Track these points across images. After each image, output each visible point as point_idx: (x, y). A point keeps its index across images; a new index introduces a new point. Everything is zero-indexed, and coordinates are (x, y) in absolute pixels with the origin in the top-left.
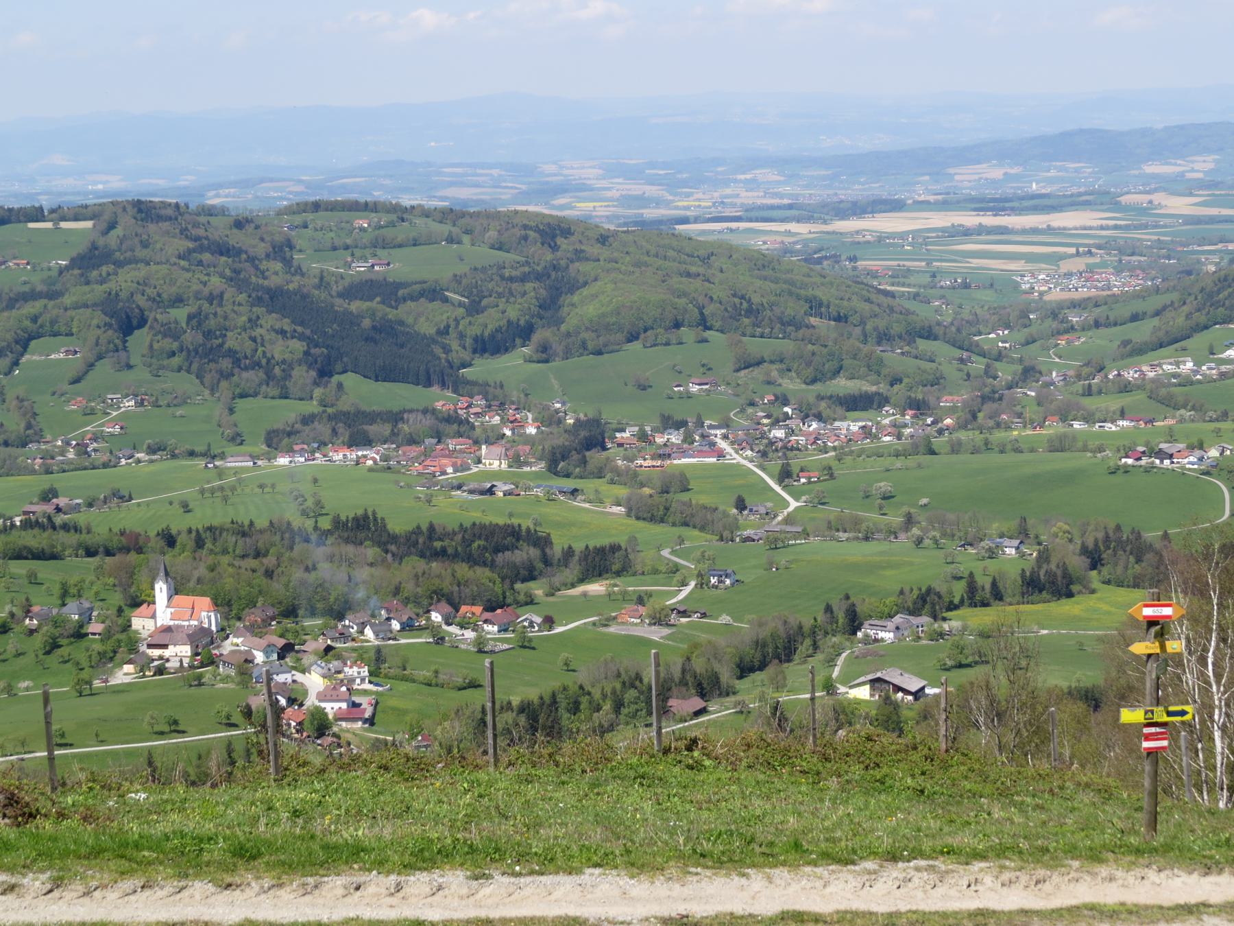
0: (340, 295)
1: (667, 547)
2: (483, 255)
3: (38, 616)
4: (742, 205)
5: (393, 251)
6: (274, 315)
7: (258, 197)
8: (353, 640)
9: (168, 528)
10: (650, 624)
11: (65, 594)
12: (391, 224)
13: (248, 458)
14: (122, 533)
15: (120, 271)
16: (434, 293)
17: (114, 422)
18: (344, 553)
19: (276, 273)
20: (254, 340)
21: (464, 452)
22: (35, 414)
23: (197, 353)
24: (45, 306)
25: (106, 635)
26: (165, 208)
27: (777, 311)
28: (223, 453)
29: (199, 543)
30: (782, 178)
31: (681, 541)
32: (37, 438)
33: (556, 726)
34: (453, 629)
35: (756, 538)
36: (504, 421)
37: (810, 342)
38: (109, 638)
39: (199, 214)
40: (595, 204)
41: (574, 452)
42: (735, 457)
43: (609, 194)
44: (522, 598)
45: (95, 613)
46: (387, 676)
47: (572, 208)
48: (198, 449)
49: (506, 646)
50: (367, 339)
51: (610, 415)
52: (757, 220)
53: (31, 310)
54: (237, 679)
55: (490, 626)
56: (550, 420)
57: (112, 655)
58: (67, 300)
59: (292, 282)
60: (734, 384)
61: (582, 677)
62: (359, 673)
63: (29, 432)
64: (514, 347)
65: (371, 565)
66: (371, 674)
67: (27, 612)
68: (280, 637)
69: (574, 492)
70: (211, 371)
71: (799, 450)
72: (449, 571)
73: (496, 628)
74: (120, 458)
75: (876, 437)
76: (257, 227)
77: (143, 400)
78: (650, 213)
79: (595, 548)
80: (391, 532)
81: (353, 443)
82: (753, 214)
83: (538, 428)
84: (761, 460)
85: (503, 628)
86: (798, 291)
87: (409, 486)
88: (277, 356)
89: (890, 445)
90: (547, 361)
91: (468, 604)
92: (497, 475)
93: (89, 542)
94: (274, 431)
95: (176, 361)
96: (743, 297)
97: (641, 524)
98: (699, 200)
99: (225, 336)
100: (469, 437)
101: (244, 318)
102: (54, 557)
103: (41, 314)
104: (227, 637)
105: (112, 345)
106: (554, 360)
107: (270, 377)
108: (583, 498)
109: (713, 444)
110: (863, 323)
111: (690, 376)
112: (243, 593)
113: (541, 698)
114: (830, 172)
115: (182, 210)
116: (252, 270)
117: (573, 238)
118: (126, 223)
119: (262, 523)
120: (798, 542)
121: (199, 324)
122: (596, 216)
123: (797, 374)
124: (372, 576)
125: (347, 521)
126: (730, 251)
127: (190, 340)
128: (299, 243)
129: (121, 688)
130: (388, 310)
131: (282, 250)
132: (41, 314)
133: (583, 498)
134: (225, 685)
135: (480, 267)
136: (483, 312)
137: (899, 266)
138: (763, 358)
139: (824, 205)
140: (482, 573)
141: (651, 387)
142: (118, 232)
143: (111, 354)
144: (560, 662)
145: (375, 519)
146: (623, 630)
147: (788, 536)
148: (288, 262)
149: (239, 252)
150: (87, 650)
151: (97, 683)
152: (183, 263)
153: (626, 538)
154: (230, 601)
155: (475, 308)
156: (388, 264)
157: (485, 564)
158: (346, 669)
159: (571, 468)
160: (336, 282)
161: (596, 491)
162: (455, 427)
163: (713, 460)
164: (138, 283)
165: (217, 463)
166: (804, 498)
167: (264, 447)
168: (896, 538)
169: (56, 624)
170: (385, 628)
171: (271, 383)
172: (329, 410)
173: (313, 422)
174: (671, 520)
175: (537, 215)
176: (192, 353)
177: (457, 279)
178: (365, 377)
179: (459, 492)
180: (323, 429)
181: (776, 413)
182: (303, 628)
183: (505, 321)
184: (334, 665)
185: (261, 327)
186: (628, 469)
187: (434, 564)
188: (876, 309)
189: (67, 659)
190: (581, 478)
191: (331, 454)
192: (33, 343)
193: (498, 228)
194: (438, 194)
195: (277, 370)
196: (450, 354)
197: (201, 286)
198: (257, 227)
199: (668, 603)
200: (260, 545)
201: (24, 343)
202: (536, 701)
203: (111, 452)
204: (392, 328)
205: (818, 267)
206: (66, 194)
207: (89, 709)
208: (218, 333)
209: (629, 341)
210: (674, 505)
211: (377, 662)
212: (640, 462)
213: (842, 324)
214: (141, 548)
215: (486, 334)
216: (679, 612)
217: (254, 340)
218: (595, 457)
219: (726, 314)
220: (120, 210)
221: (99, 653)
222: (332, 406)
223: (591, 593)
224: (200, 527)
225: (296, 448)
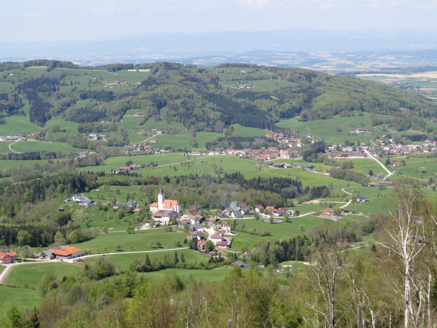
0: (235, 96)
1: (343, 188)
2: (284, 83)
3: (118, 205)
4: (380, 67)
5: (254, 81)
6: (211, 103)
7: (210, 62)
8: (227, 217)
9: (167, 176)
10: (334, 215)
11: (128, 198)
12: (253, 72)
13: (199, 152)
14: (152, 177)
15: (158, 86)
16: (267, 96)
17: (154, 139)
18: (227, 187)
19: (212, 88)
20: (203, 111)
21: (275, 152)
22: (127, 135)
23: (183, 115)
24: (132, 98)
25: (141, 212)
26: (175, 65)
27: (389, 105)
28: (191, 150)
29: (178, 182)
30: (395, 59)
31: (348, 186)
32: (127, 143)
33: (294, 251)
34: (263, 215)
35: (375, 185)
36: (290, 142)
37: (400, 116)
38: (141, 213)
39: (187, 67)
40: (329, 67)
41: (313, 153)
42: (372, 157)
43: (333, 63)
44: (289, 204)
45: (138, 205)
46: (237, 230)
47: (319, 68)
48: (182, 149)
49: (281, 221)
50: (243, 112)
51: (327, 141)
52: (385, 73)
53: (128, 99)
54: (184, 230)
55: (276, 214)
56: (306, 142)
57: (142, 220)
58: (140, 96)
59: (218, 91)
60: (372, 131)
61: (307, 233)
62: (227, 229)
63: (125, 141)
64: (294, 116)
65: (237, 191)
66: (231, 229)
67: (115, 204)
68: (201, 215)
69: (312, 167)
70: (188, 122)
71: (394, 154)
72: (264, 194)
73: (278, 215)
74: (155, 151)
75: (422, 151)
76: (206, 72)
77: (164, 131)
78: (347, 70)
79: (317, 187)
80: (245, 180)
81: (236, 148)
82: (384, 71)
83: (302, 144)
84: (380, 158)
85: (281, 214)
86: (397, 98)
87: (254, 164)
88: (211, 117)
89: (426, 154)
90: (306, 121)
91: (269, 206)
92: (285, 161)
93: (140, 180)
94: (209, 143)
95: (176, 118)
96: (376, 100)
97: (335, 179)
98: (365, 66)
99: (193, 110)
100: (277, 147)
101: (200, 104)
102: (127, 185)
103: (131, 101)
104: (183, 215)
105: (154, 112)
106: (308, 121)
107: (208, 124)
108: (315, 169)
109: (363, 152)
110: (419, 110)
111: (356, 127)
112: (190, 199)
113: (290, 240)
114: (412, 57)
115: (181, 66)
116: (204, 87)
117: (317, 78)
118: (162, 71)
119: (200, 175)
120: (390, 187)
121: (185, 105)
122: (328, 71)
123: (395, 128)
124: (236, 195)
125: (230, 175)
126: (373, 84)
127: (181, 111)
128: (221, 78)
129: (144, 231)
130: (251, 102)
131: (215, 80)
132: (131, 101)
133: (315, 169)
134: (180, 232)
135: (283, 87)
136: (284, 103)
137: (435, 90)
138: (383, 121)
139: (409, 68)
140: (275, 195)
141: (342, 131)
142: (159, 73)
143: (154, 115)
144: (300, 228)
145: (240, 175)
146: (324, 217)
147: (387, 185)
148: (217, 85)
149: (200, 80)
150: (133, 218)
151: (136, 229)
152: (180, 84)
153: (329, 184)
154: (185, 202)
155: (281, 102)
156: (252, 86)
157: (277, 192)
158: (223, 227)
159: (312, 159)
160: (233, 92)
161: (320, 167)
162: (272, 143)
163: (363, 157)
164: (164, 91)
165: (188, 154)
166: (394, 172)
167: (205, 149)
168: (426, 187)
169: (124, 208)
170: (239, 213)
171: (209, 127)
172: (228, 136)
173: (222, 140)
174: (346, 178)
175: (307, 70)
176: (182, 115)
177: (275, 91)
178: (242, 125)
179: (271, 166)
180: (226, 143)
181: (387, 141)
182: (210, 212)
183: (291, 107)
184: (219, 226)
185: (206, 107)
186: (332, 160)
187: (258, 191)
188: (425, 105)
189: (127, 220)
190: (315, 162)
191: (228, 152)
192: (128, 111)
193: (291, 74)
194: (273, 62)
195: (211, 122)
196: (272, 118)
197: (186, 92)
198: (206, 72)
199: (340, 208)
200: (199, 183)
201: (124, 111)
202: (288, 241)
203: (152, 149)
204: (252, 108)
205: (405, 90)
206: (145, 60)
207: (132, 238)
208: (191, 109)
209: (335, 115)
210: (347, 173)
211: (234, 226)
212: (337, 157)
213: (412, 110)
214: (158, 183)
215: (285, 111)
216: (345, 211)
217: (203, 111)
218: (321, 155)
219: (370, 106)
220: (159, 66)
221: (137, 219)
222: (230, 135)
223: (314, 203)
224: (179, 176)
225: (216, 149)
